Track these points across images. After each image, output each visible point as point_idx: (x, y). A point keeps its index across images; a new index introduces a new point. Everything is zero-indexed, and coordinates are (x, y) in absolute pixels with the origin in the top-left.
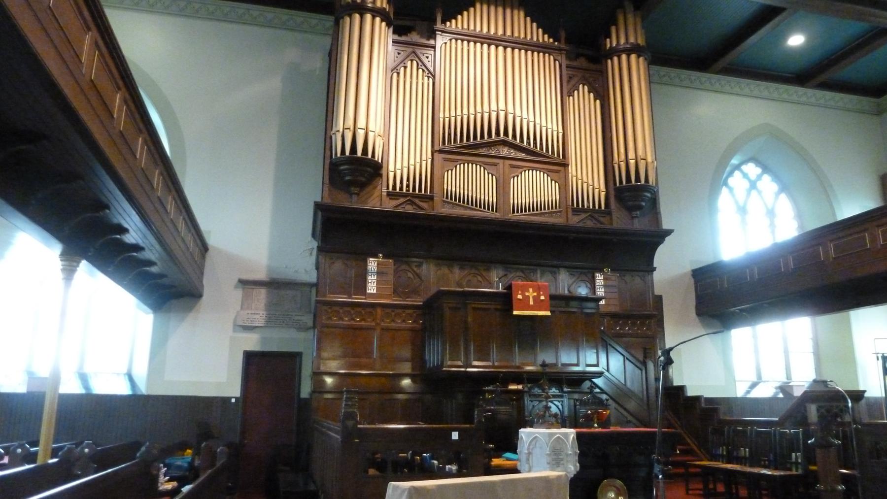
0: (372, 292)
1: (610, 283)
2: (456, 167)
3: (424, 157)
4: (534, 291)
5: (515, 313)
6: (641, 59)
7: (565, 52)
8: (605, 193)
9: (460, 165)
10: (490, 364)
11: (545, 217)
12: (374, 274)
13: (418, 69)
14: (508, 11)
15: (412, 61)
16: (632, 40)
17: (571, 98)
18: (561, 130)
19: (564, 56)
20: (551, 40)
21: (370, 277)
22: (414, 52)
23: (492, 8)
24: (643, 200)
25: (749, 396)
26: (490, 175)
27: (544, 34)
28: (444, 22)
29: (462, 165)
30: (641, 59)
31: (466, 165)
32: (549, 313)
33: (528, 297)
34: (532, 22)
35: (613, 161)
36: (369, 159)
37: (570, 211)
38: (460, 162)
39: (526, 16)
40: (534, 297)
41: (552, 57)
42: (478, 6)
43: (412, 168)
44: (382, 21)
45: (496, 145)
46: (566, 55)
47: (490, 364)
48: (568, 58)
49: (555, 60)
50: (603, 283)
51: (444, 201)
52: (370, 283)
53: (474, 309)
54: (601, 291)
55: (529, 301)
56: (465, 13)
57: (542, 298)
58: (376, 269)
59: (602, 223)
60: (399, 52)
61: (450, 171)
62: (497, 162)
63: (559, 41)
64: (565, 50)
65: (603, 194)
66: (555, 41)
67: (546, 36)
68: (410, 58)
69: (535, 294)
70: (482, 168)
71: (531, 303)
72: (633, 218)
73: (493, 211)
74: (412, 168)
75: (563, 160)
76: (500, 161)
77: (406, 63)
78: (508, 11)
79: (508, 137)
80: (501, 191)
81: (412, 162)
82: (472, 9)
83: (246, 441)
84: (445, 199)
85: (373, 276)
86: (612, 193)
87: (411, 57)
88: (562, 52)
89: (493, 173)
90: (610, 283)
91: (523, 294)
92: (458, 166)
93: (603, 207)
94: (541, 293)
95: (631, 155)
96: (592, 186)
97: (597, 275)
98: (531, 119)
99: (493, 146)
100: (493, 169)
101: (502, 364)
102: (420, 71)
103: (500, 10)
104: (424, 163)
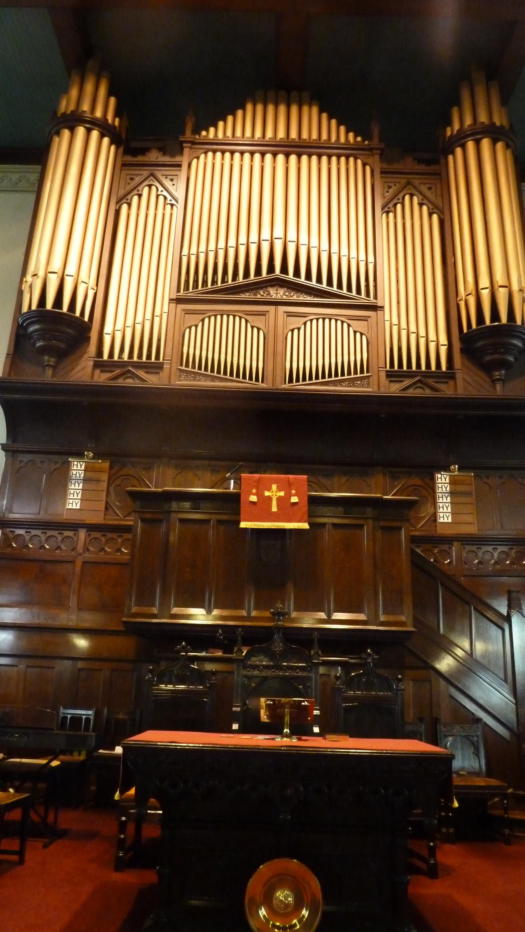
0: (446, 520)
1: (461, 488)
2: (203, 321)
3: (158, 312)
4: (279, 489)
5: (243, 525)
6: (500, 146)
7: (378, 152)
8: (446, 347)
9: (209, 317)
10: (362, 617)
11: (341, 386)
12: (79, 481)
13: (158, 196)
14: (294, 109)
15: (150, 186)
16: (483, 118)
17: (391, 215)
18: (371, 259)
19: (377, 158)
20: (359, 139)
21: (73, 485)
22: (152, 175)
23: (271, 108)
24: (508, 352)
25: (454, 776)
26: (255, 330)
27: (347, 132)
28: (197, 131)
29: (213, 318)
30: (500, 146)
31: (219, 317)
32: (305, 526)
33: (270, 498)
34: (330, 119)
35: (457, 296)
36: (77, 317)
37: (383, 374)
38: (209, 314)
39: (320, 112)
40: (279, 499)
41: (359, 162)
42: (249, 107)
43: (138, 328)
44: (111, 143)
45: (266, 287)
46: (381, 156)
47: (362, 617)
48: (383, 157)
49: (364, 165)
50: (448, 489)
51: (181, 371)
52: (72, 495)
53: (182, 521)
54: (445, 500)
55: (270, 506)
56: (230, 118)
57: (294, 499)
58: (82, 475)
59: (436, 390)
60: (132, 177)
61: (193, 328)
62: (266, 310)
63: (370, 139)
64: (377, 149)
65: (443, 350)
66: (364, 140)
67: (351, 135)
68: (146, 183)
69: (282, 494)
70: (243, 321)
71: (274, 509)
72: (494, 381)
73: (258, 381)
74: (138, 328)
75: (375, 301)
76: (272, 308)
77: (141, 189)
78: (294, 109)
79: (287, 274)
80: (270, 350)
81: (139, 319)
82: (240, 113)
83: (225, 691)
84: (184, 368)
85: (77, 484)
86: (457, 345)
87: (149, 181)
88: (374, 151)
89: (260, 326)
90: (461, 488)
91: (260, 495)
92: (207, 320)
93: (444, 368)
94: (294, 492)
95: (484, 282)
96: (415, 335)
97: (439, 476)
98: (325, 246)
99: (261, 288)
100: (259, 321)
101: (392, 618)
102: (161, 198)
103: (282, 109)
104: (157, 320)
